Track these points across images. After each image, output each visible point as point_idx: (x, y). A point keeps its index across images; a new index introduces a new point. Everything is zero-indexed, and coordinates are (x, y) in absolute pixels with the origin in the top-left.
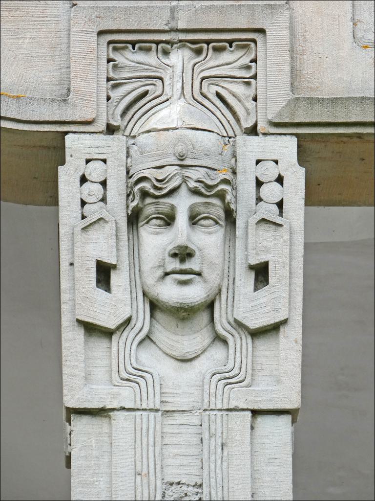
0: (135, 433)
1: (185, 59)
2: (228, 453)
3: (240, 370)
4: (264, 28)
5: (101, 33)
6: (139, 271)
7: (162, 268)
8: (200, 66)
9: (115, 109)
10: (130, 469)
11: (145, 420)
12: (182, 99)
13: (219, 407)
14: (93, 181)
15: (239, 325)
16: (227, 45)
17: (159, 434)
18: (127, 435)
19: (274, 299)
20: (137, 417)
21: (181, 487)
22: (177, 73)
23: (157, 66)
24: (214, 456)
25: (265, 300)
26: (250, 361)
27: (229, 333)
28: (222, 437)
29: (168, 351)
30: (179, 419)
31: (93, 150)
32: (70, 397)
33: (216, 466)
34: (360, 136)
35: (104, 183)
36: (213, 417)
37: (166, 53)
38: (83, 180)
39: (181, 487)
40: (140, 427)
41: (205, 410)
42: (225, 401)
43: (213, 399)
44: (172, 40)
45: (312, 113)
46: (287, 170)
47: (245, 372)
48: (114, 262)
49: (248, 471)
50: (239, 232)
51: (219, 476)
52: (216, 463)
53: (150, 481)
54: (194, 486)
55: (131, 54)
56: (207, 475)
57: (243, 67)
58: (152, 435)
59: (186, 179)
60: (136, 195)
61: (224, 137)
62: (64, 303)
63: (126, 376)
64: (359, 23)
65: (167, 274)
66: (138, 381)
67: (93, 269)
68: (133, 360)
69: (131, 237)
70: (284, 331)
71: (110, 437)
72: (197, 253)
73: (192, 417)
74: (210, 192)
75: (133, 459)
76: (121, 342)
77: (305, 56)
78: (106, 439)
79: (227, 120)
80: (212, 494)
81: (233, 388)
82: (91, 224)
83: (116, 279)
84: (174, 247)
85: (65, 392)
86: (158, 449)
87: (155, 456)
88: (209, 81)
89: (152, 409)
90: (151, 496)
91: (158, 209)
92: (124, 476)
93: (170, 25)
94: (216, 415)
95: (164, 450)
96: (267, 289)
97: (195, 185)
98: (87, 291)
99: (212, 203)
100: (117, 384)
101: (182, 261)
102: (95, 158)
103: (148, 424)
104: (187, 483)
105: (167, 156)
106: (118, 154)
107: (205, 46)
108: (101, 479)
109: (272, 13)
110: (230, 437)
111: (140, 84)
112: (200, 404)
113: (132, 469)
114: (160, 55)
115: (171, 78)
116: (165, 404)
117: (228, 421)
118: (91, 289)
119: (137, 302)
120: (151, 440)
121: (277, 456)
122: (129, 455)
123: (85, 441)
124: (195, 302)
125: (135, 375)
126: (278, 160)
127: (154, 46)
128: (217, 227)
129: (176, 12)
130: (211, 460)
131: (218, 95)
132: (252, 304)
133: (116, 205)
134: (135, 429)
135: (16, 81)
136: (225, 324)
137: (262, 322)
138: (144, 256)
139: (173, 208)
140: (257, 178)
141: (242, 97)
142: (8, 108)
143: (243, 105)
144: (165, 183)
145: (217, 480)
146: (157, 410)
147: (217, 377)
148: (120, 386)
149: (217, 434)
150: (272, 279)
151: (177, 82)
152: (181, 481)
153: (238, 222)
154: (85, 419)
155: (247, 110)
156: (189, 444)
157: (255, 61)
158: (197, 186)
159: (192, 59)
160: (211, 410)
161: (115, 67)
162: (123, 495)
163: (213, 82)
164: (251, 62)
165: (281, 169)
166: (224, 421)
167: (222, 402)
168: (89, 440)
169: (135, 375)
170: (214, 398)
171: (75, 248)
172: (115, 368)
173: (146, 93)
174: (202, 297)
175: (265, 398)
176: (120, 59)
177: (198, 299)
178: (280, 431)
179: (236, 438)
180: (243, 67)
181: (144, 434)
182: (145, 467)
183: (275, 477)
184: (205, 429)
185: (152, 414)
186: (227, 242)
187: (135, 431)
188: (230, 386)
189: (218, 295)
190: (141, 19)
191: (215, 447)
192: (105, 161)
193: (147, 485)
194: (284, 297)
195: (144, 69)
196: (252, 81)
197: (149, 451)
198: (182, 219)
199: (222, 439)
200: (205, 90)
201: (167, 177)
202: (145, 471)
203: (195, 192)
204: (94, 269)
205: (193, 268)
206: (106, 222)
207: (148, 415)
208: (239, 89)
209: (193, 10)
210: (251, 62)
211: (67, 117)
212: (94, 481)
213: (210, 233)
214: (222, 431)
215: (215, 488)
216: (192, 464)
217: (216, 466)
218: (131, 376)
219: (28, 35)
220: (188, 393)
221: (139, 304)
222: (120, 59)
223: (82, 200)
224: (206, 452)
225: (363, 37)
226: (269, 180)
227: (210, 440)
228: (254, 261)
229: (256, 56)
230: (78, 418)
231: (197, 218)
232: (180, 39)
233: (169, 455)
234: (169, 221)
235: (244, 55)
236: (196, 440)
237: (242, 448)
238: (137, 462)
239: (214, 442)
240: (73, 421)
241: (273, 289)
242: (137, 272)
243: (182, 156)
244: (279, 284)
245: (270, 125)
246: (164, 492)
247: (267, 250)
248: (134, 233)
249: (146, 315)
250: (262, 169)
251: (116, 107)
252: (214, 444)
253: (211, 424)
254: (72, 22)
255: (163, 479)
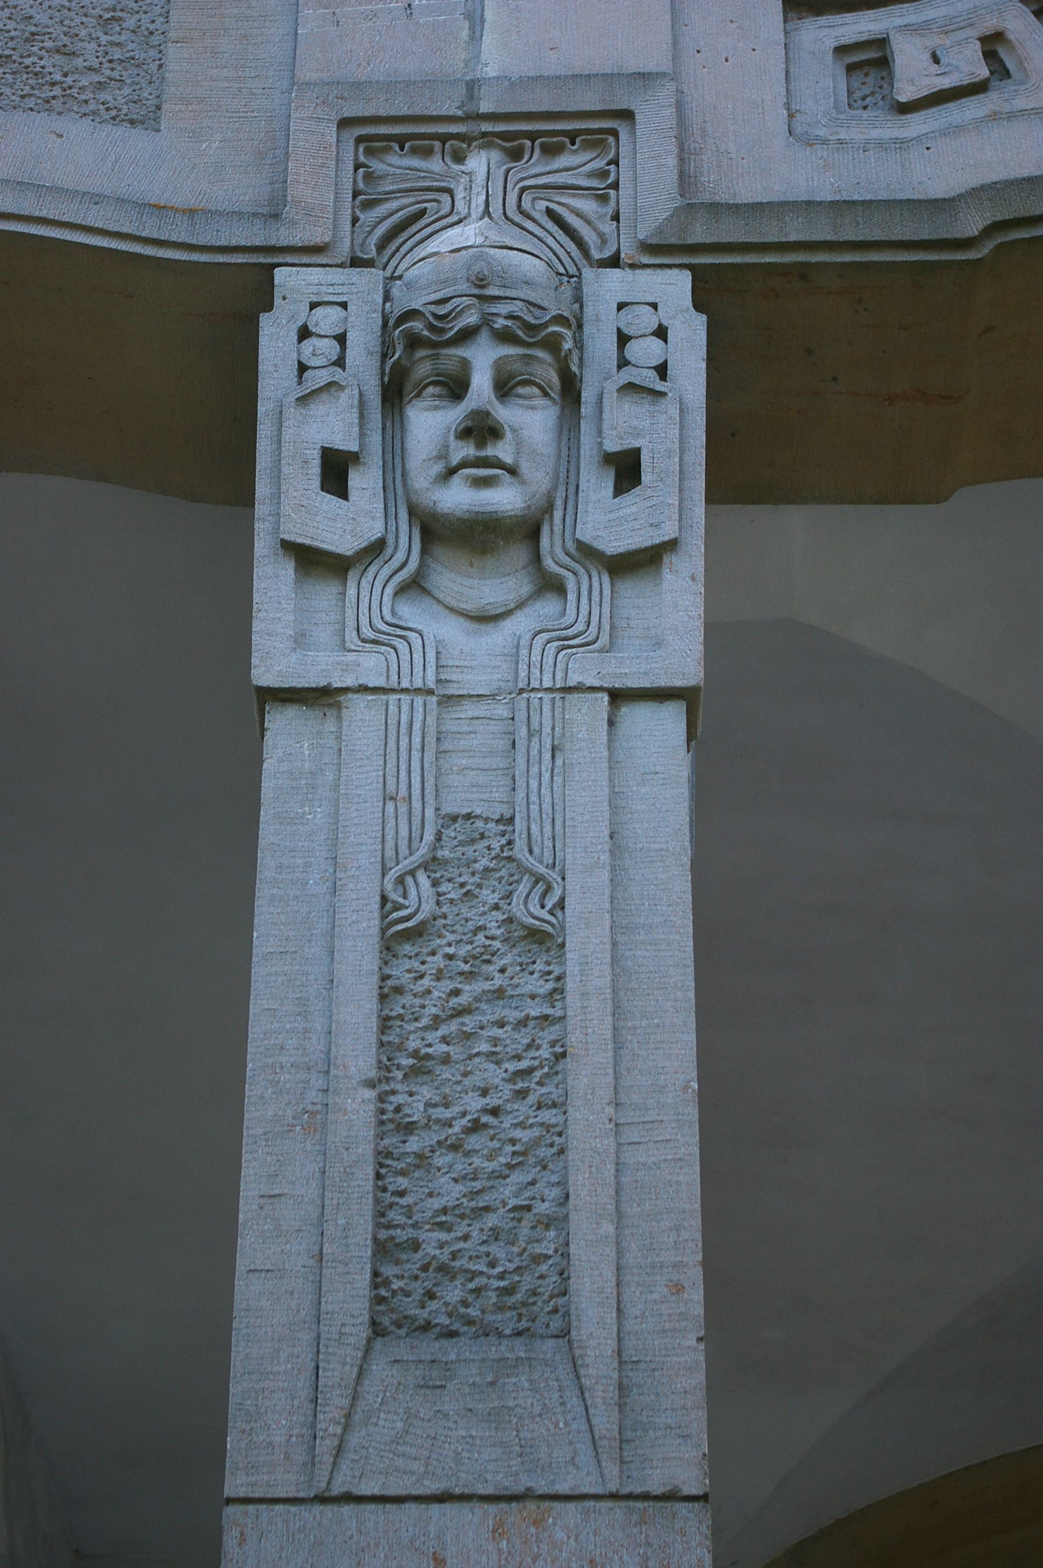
0: (386, 730)
1: (492, 162)
2: (564, 761)
3: (588, 626)
4: (632, 108)
5: (344, 123)
6: (402, 476)
7: (444, 461)
8: (518, 172)
9: (367, 237)
10: (374, 790)
11: (405, 708)
12: (486, 219)
13: (547, 683)
14: (322, 333)
15: (587, 553)
16: (567, 140)
17: (432, 731)
18: (371, 732)
19: (651, 507)
20: (390, 703)
21: (472, 824)
22: (478, 181)
23: (443, 173)
24: (537, 766)
25: (634, 509)
26: (606, 609)
27: (568, 570)
28: (553, 736)
29: (454, 604)
30: (469, 710)
31: (324, 289)
32: (263, 669)
33: (540, 784)
34: (803, 271)
35: (341, 339)
36: (536, 703)
37: (459, 158)
38: (304, 333)
39: (472, 824)
40: (396, 719)
41: (522, 691)
42: (559, 675)
43: (536, 672)
44: (469, 134)
45: (718, 228)
46: (673, 317)
47: (597, 628)
48: (354, 447)
49: (603, 791)
50: (586, 409)
51: (546, 800)
52: (540, 779)
53: (413, 810)
54: (497, 821)
55: (396, 157)
56: (523, 798)
57: (590, 175)
58: (419, 733)
59: (489, 318)
60: (397, 342)
61: (561, 275)
62: (259, 519)
63: (370, 634)
64: (798, 114)
65: (451, 472)
66: (394, 643)
67: (314, 461)
68: (386, 611)
69: (389, 424)
70: (671, 562)
71: (339, 738)
72: (508, 434)
73: (497, 706)
74: (532, 337)
75: (381, 773)
76: (363, 583)
77: (704, 157)
78: (331, 741)
79: (566, 251)
80: (532, 832)
81: (574, 654)
82: (314, 392)
83: (355, 479)
84: (465, 417)
85: (254, 661)
86: (429, 756)
87: (422, 768)
88: (535, 193)
89: (420, 689)
90: (414, 835)
91: (438, 366)
92: (361, 800)
93: (465, 108)
94: (541, 698)
95: (442, 761)
96: (637, 493)
97: (573, 857)
98: (302, 496)
99: (536, 357)
100: (353, 647)
101: (481, 444)
102: (325, 299)
103: (412, 716)
104: (484, 816)
105: (456, 282)
106: (369, 294)
107: (528, 143)
108: (319, 810)
109: (645, 86)
110: (567, 734)
111: (411, 200)
112: (511, 684)
113: (378, 790)
114: (448, 160)
115: (466, 189)
116: (445, 684)
117: (564, 708)
118: (310, 492)
119: (397, 522)
120: (417, 740)
121: (658, 769)
122: (372, 766)
123: (290, 746)
124: (503, 512)
125: (389, 634)
126: (657, 303)
127: (437, 144)
128: (546, 402)
129: (476, 88)
130: (531, 773)
131: (550, 213)
132: (612, 516)
133: (361, 369)
134: (386, 723)
135: (193, 201)
136: (559, 556)
137: (628, 544)
138: (411, 444)
139: (465, 365)
140: (619, 330)
141: (593, 217)
142: (174, 227)
143: (595, 229)
144: (450, 321)
145: (543, 807)
146: (430, 692)
147: (545, 636)
148: (359, 651)
149: (544, 730)
150: (645, 478)
151: (478, 194)
152: (473, 812)
153: (584, 395)
154: (291, 712)
155: (601, 235)
156: (489, 750)
157: (615, 162)
158: (510, 324)
159: (504, 164)
160: (533, 690)
161: (369, 177)
162: (360, 834)
163: (543, 196)
164: (608, 164)
165: (664, 315)
166: (556, 708)
167: (554, 678)
168: (299, 745)
169: (389, 634)
170: (539, 670)
171: (283, 429)
172: (351, 623)
173: (423, 212)
174: (517, 506)
175: (635, 670)
176: (377, 166)
177: (509, 507)
178: (665, 726)
179: (580, 736)
180: (590, 175)
181: (403, 730)
182: (403, 786)
183: (654, 805)
184: (521, 721)
185: (419, 701)
186: (565, 432)
187: (386, 727)
188: (569, 651)
189: (547, 512)
190: (415, 99)
191: (540, 752)
192: (344, 305)
193: (406, 817)
194: (670, 504)
195: (419, 177)
196: (612, 192)
197: (413, 758)
198: (481, 382)
199: (553, 740)
200: (526, 205)
201: (453, 310)
202: (403, 792)
203: (505, 337)
204: (316, 463)
205: (500, 457)
206: (342, 388)
207: (413, 700)
208: (587, 205)
209: (507, 83)
210: (608, 164)
211: (278, 240)
212: (304, 813)
213: (532, 408)
214: (554, 725)
215: (539, 822)
216: (494, 784)
217: (540, 784)
218: (381, 636)
219: (218, 136)
220: (489, 667)
221: (400, 524)
222: (377, 166)
223: (300, 363)
224: (521, 761)
225: (806, 132)
226: (640, 333)
227: (530, 741)
228: (612, 446)
229: (618, 154)
230: (279, 708)
231: (510, 385)
232: (483, 130)
233: (451, 769)
234: (458, 391)
235: (595, 158)
236: (503, 744)
237: (590, 752)
238: (388, 778)
239: (538, 744)
240: (268, 712)
241: (649, 493)
242: (398, 476)
243: (482, 280)
244: (659, 483)
245: (642, 251)
246: (440, 831)
247: (638, 434)
248: (395, 419)
249: (413, 543)
250: (629, 317)
251: (369, 234)
252: (537, 746)
253: (532, 714)
254: (293, 105)
255: (437, 809)
